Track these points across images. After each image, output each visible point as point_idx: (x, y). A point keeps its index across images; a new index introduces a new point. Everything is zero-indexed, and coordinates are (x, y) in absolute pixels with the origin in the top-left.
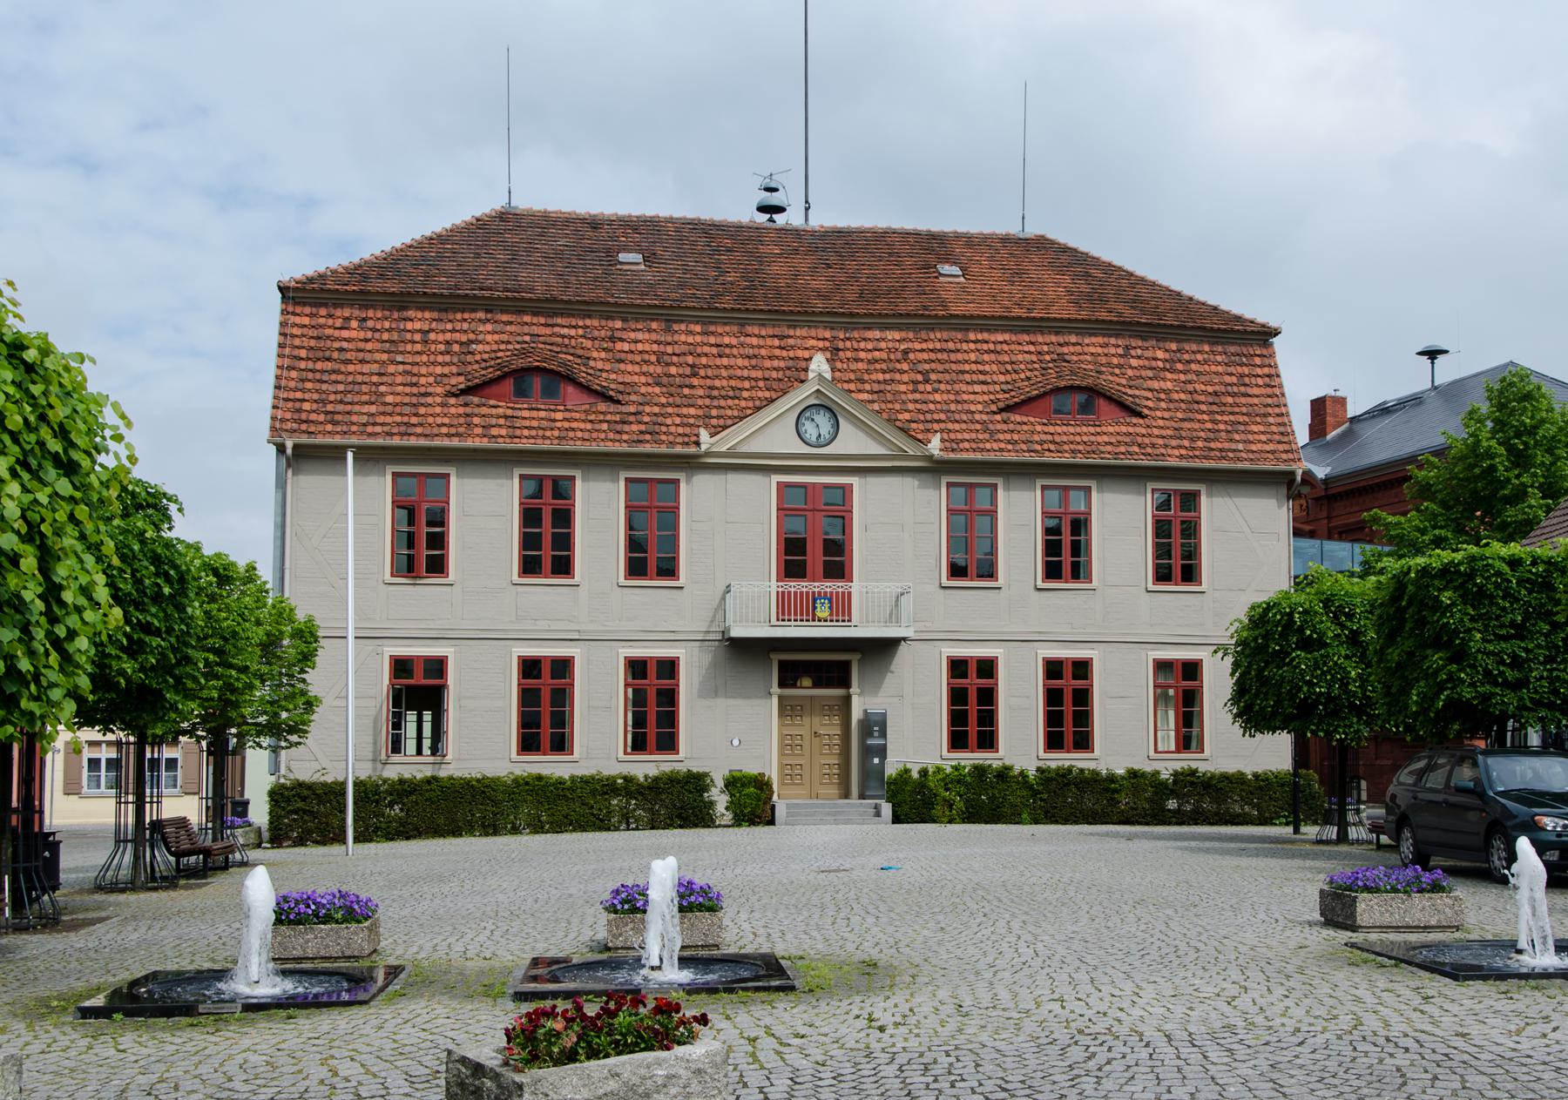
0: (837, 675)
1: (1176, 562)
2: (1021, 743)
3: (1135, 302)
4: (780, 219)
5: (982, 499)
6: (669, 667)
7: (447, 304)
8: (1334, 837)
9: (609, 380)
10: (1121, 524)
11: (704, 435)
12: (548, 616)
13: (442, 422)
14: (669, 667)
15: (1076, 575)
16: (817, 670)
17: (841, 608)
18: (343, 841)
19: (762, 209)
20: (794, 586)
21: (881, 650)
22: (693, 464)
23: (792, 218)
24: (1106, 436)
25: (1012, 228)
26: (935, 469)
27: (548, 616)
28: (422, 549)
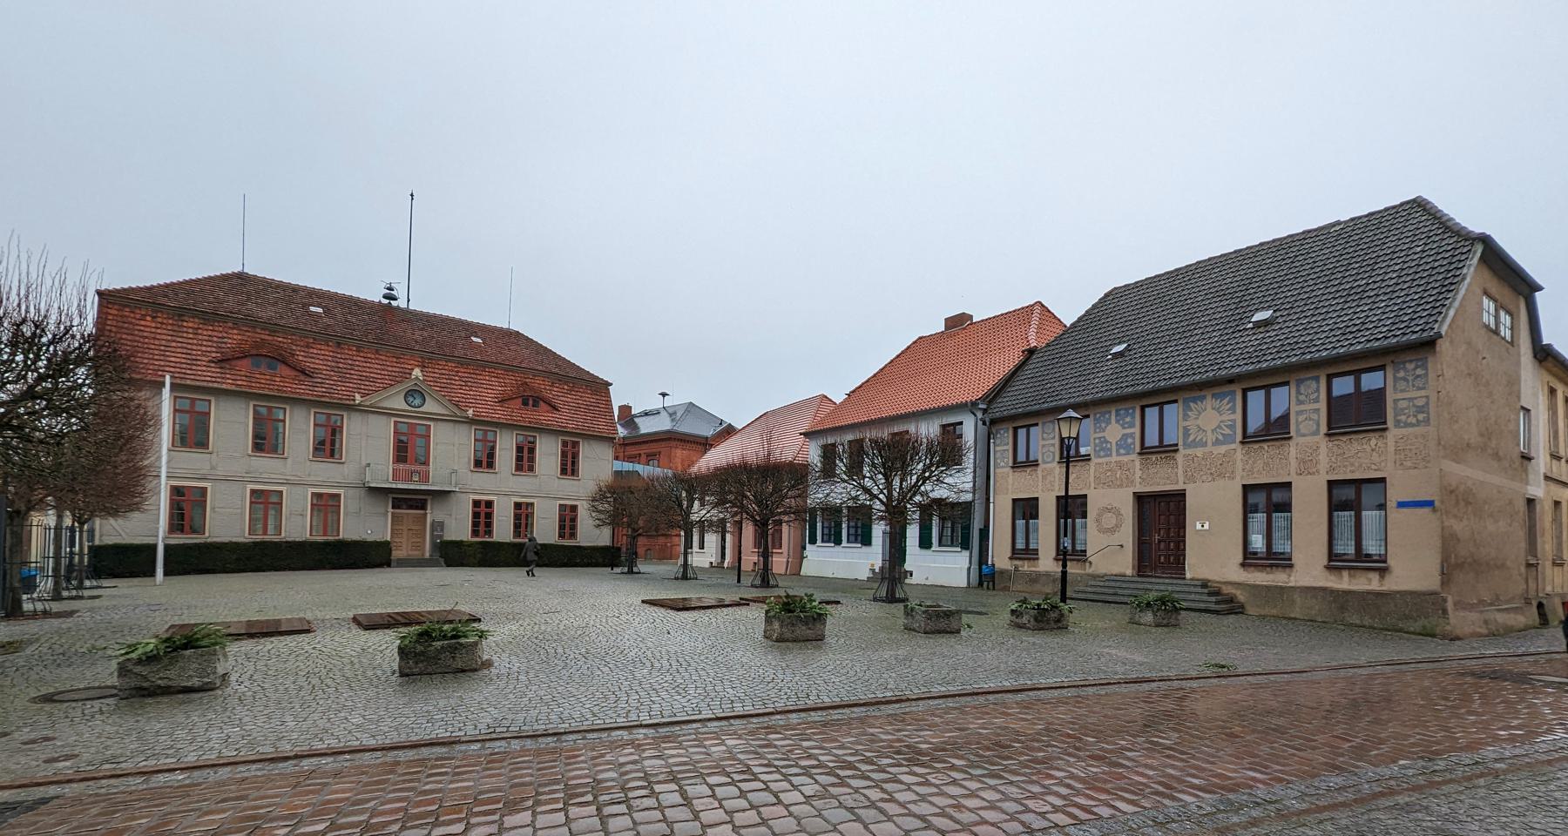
0: (422, 505)
1: (569, 466)
2: (503, 530)
3: (557, 366)
4: (394, 303)
5: (490, 436)
6: (574, 508)
7: (210, 317)
8: (1339, 549)
9: (309, 364)
10: (548, 453)
11: (358, 397)
12: (522, 487)
13: (207, 375)
14: (574, 508)
15: (332, 456)
16: (410, 501)
17: (425, 478)
18: (152, 573)
19: (385, 297)
20: (401, 466)
21: (442, 495)
22: (352, 408)
23: (401, 303)
24: (544, 416)
25: (505, 326)
26: (472, 422)
27: (522, 487)
28: (485, 461)
